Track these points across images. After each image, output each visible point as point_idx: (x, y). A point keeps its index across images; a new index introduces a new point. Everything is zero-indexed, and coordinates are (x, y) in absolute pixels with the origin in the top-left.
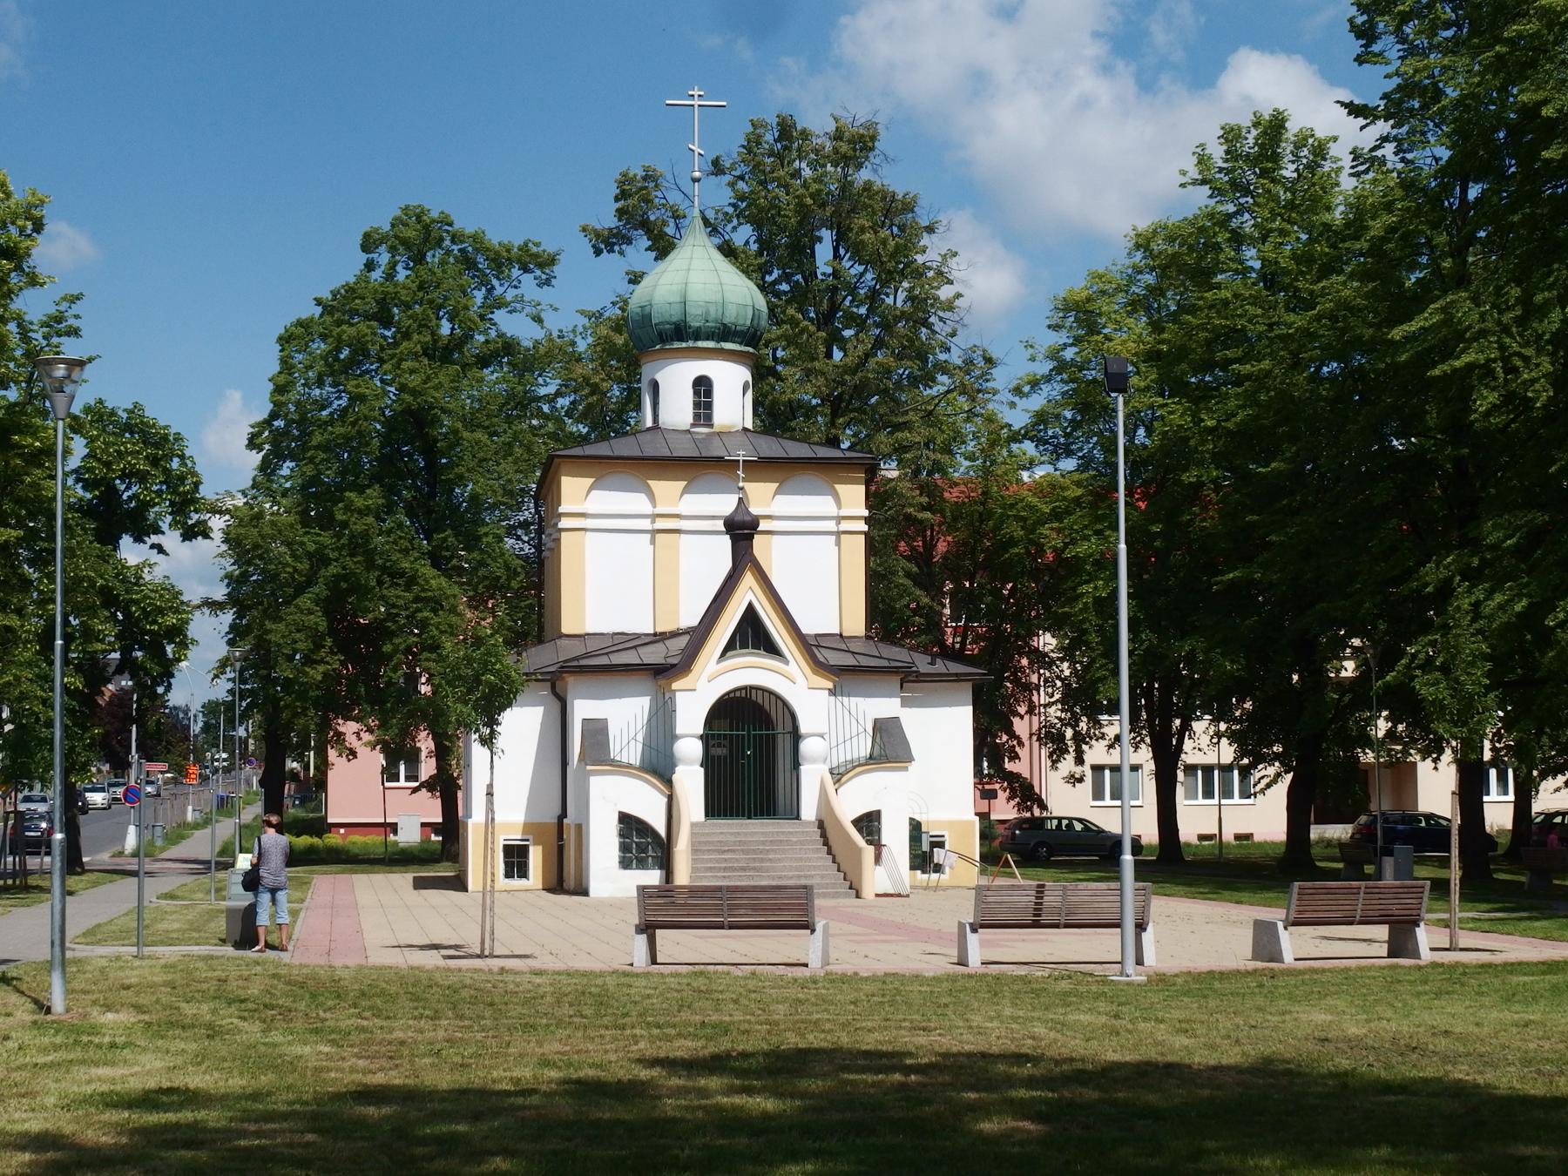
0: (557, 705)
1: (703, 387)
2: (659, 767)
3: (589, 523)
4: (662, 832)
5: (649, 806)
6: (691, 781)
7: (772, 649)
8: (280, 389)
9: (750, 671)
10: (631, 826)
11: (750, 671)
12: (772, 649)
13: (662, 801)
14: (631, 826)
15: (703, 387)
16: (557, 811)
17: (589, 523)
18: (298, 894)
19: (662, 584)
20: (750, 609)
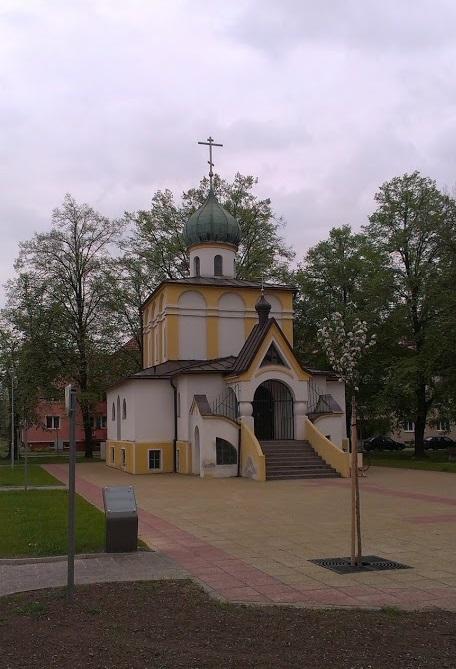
0: (172, 390)
1: (218, 259)
2: (234, 417)
3: (183, 313)
4: (235, 444)
5: (228, 433)
6: (248, 423)
7: (280, 362)
8: (446, 200)
9: (273, 373)
10: (221, 443)
11: (273, 373)
12: (280, 362)
13: (236, 432)
14: (221, 443)
15: (218, 259)
16: (173, 438)
17: (183, 313)
18: (332, 435)
19: (212, 338)
20: (273, 346)
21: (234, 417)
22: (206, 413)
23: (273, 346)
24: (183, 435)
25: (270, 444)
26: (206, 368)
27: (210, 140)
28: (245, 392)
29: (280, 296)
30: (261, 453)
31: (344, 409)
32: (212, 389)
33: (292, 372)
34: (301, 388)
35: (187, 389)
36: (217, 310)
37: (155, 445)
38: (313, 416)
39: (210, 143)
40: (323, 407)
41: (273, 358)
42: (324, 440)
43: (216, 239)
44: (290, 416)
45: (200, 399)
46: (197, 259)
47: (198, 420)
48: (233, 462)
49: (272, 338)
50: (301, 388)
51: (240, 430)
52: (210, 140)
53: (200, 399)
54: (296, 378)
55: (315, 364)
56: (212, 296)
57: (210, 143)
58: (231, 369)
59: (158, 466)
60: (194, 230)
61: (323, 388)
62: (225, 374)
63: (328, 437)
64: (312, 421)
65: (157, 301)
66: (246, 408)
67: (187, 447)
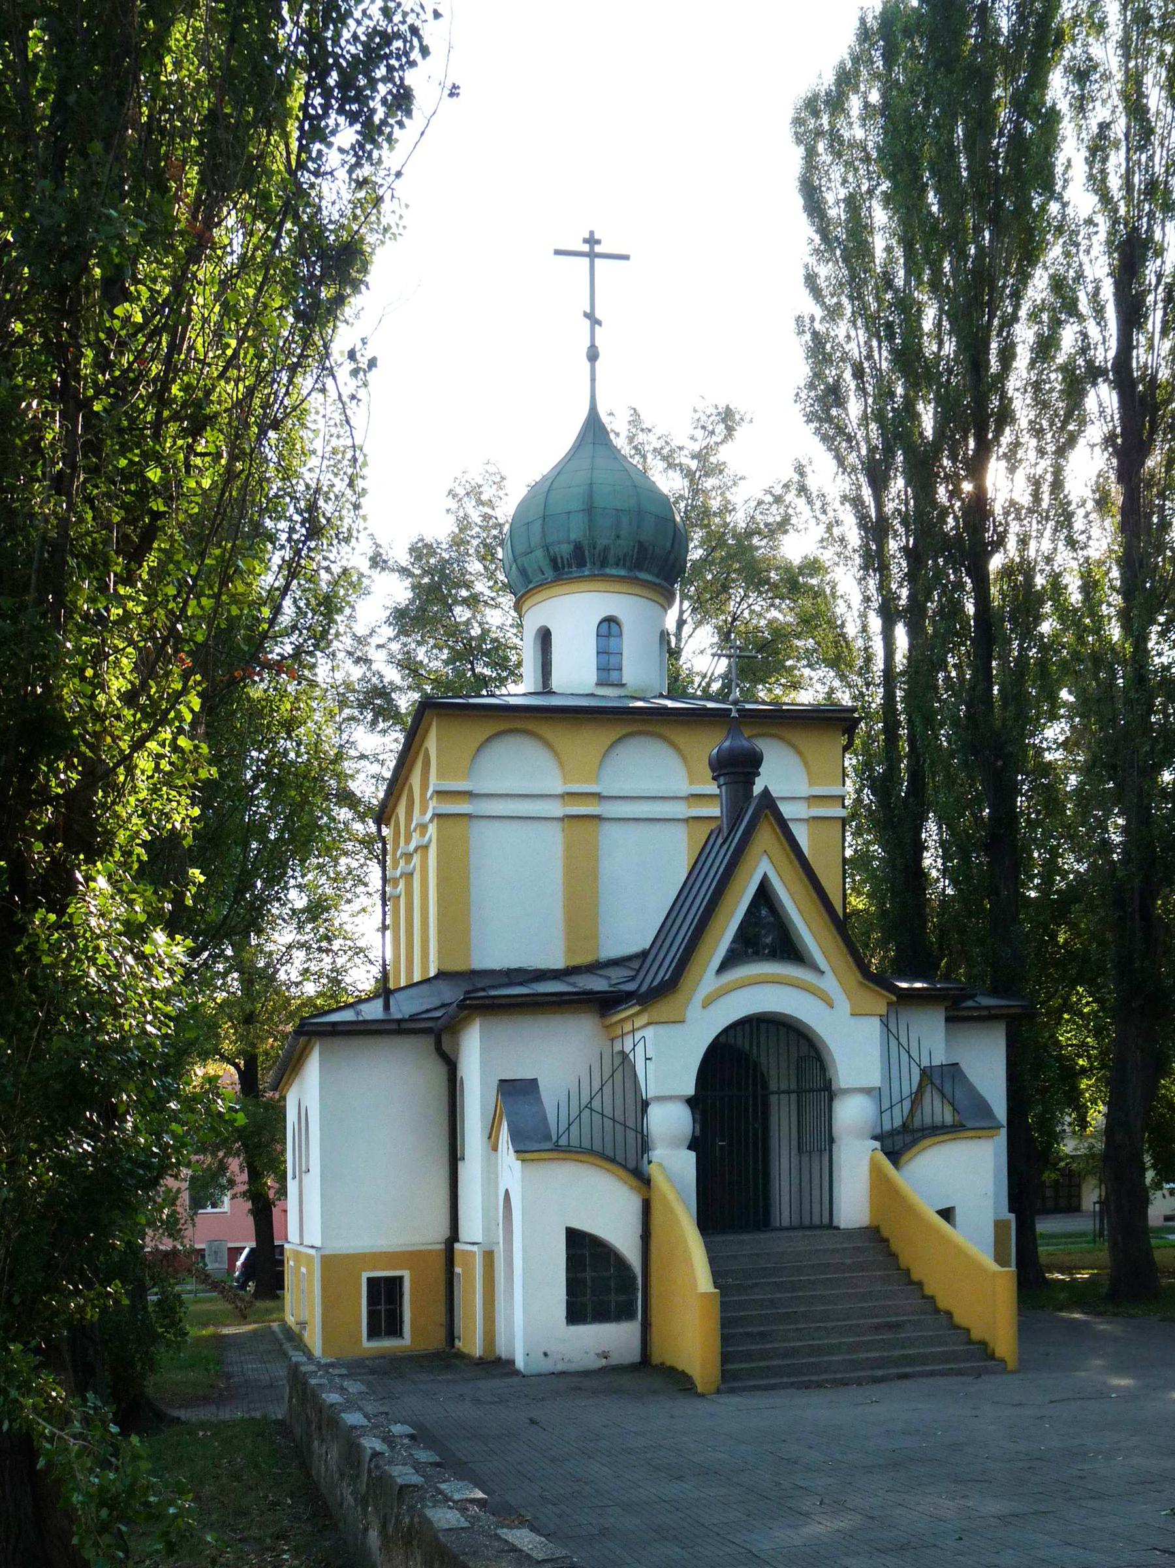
0: (438, 1072)
1: (609, 626)
2: (630, 1160)
6: (675, 1165)
7: (788, 949)
9: (765, 991)
10: (584, 1250)
11: (765, 991)
12: (788, 949)
14: (584, 1250)
20: (764, 893)
21: (630, 1160)
22: (535, 1140)
23: (764, 893)
24: (472, 1228)
25: (747, 1244)
26: (373, 1027)
27: (592, 241)
28: (668, 1057)
29: (798, 738)
30: (703, 1281)
31: (1000, 1109)
32: (559, 1058)
33: (830, 983)
34: (857, 1045)
35: (481, 1056)
36: (598, 796)
37: (392, 1258)
38: (898, 1143)
39: (591, 249)
40: (936, 1109)
41: (767, 937)
42: (930, 1227)
43: (604, 563)
44: (819, 1142)
45: (516, 1093)
46: (545, 637)
47: (511, 1170)
48: (624, 1313)
49: (764, 865)
50: (857, 1045)
51: (646, 1208)
52: (592, 241)
53: (516, 1093)
54: (843, 1005)
55: (905, 950)
56: (585, 744)
57: (591, 249)
58: (608, 993)
59: (395, 1329)
60: (536, 539)
61: (931, 1040)
62: (605, 1004)
63: (437, 15)
64: (895, 1156)
65: (415, 779)
66: (670, 1121)
67: (479, 1262)
